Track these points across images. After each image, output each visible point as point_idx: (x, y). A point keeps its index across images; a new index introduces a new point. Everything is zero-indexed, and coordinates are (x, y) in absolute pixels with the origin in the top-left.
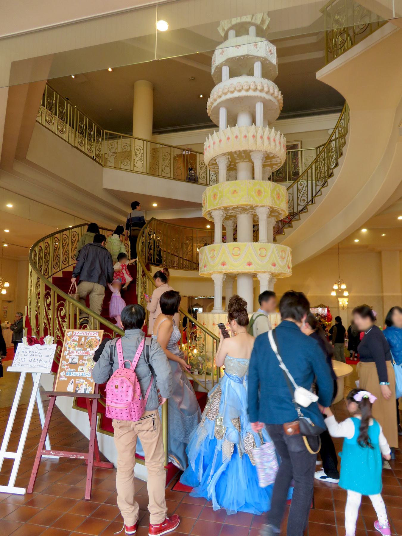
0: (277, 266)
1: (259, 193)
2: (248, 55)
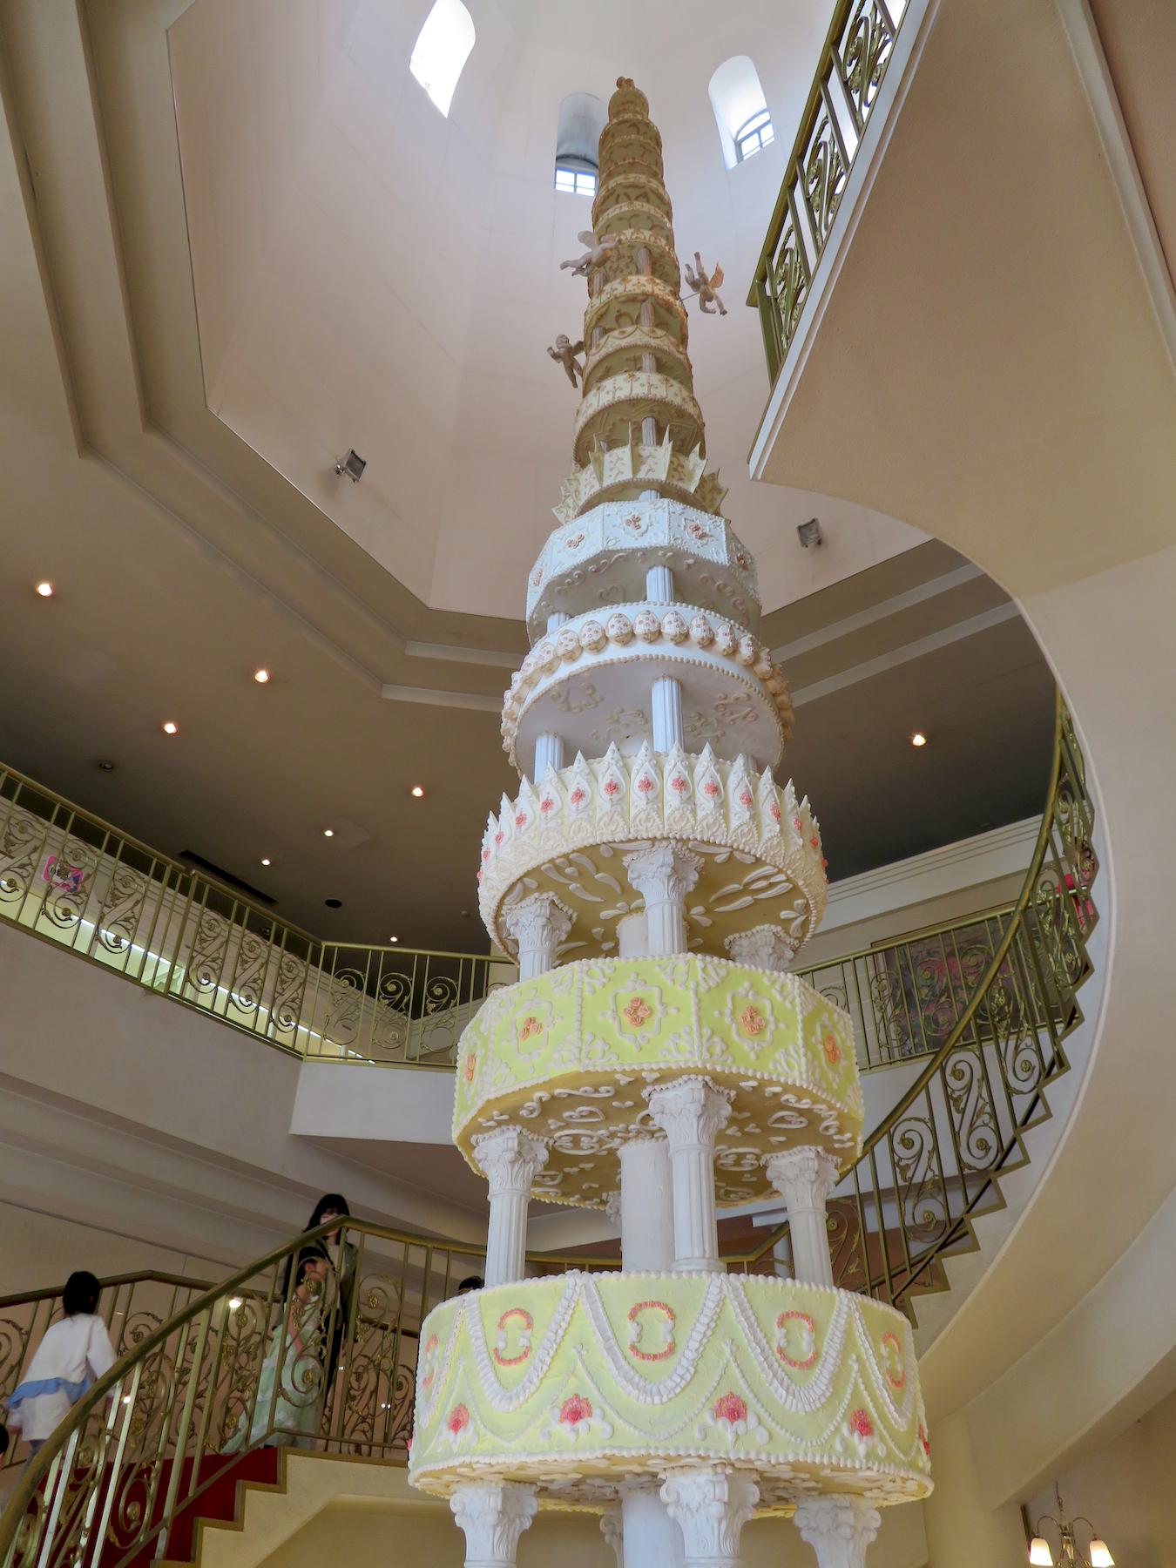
0: (751, 1419)
1: (638, 1012)
2: (607, 554)
